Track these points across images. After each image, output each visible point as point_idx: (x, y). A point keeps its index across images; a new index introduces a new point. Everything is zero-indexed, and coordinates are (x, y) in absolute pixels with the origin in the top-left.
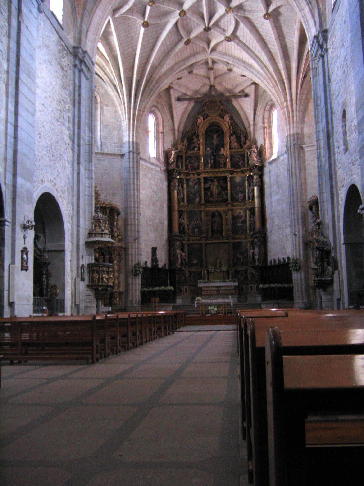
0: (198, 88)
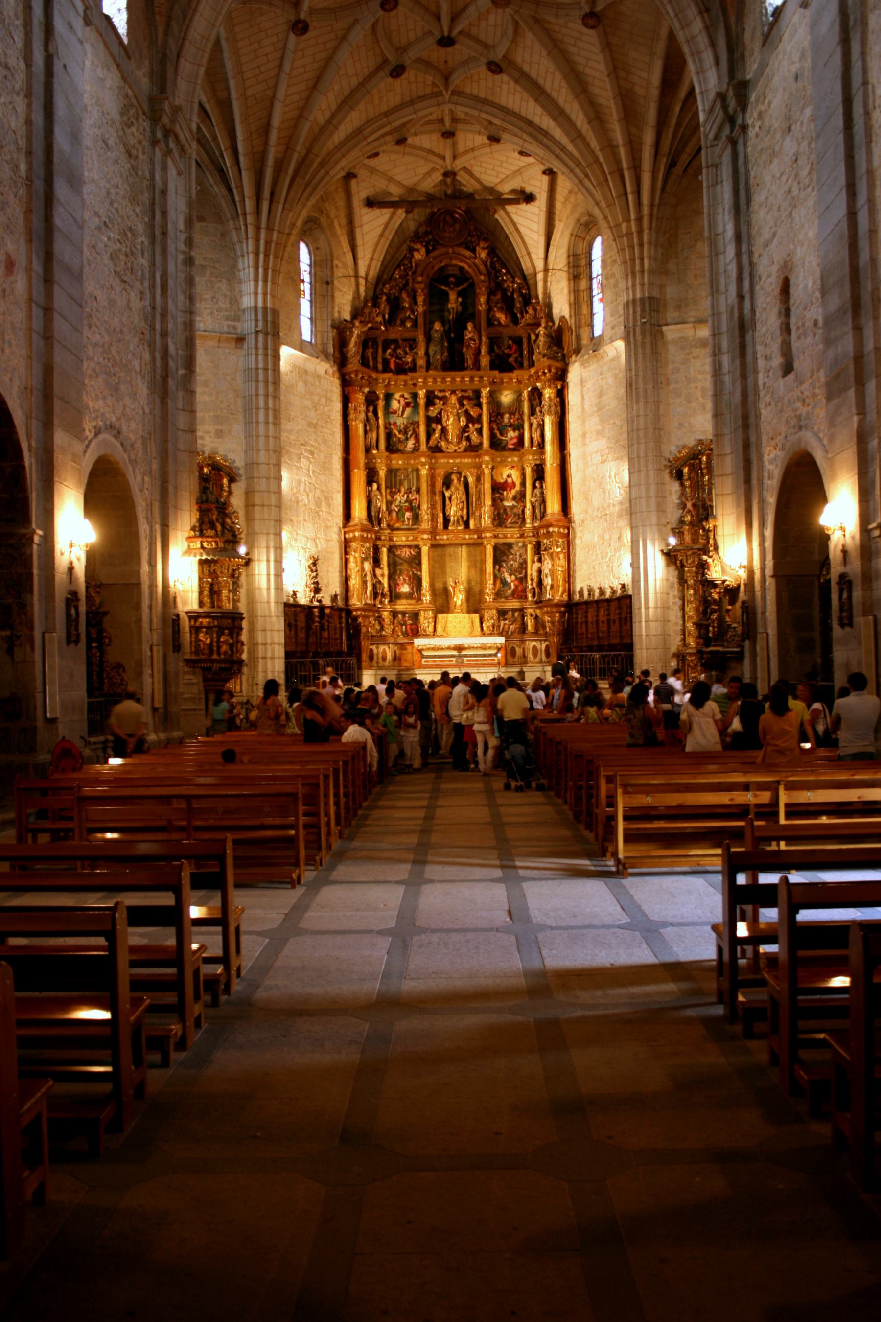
0: (414, 180)
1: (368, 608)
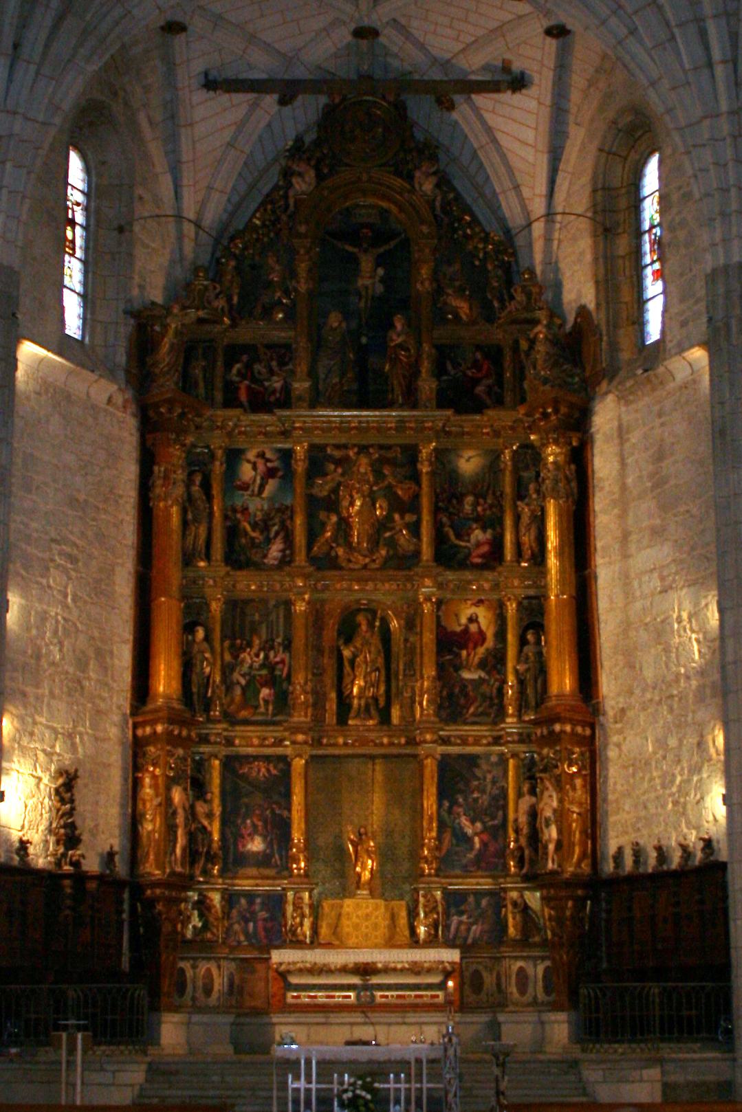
1: (182, 883)
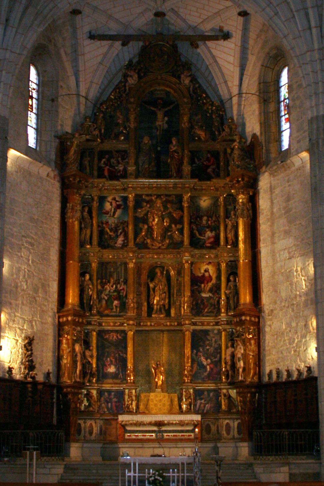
1: (80, 386)
